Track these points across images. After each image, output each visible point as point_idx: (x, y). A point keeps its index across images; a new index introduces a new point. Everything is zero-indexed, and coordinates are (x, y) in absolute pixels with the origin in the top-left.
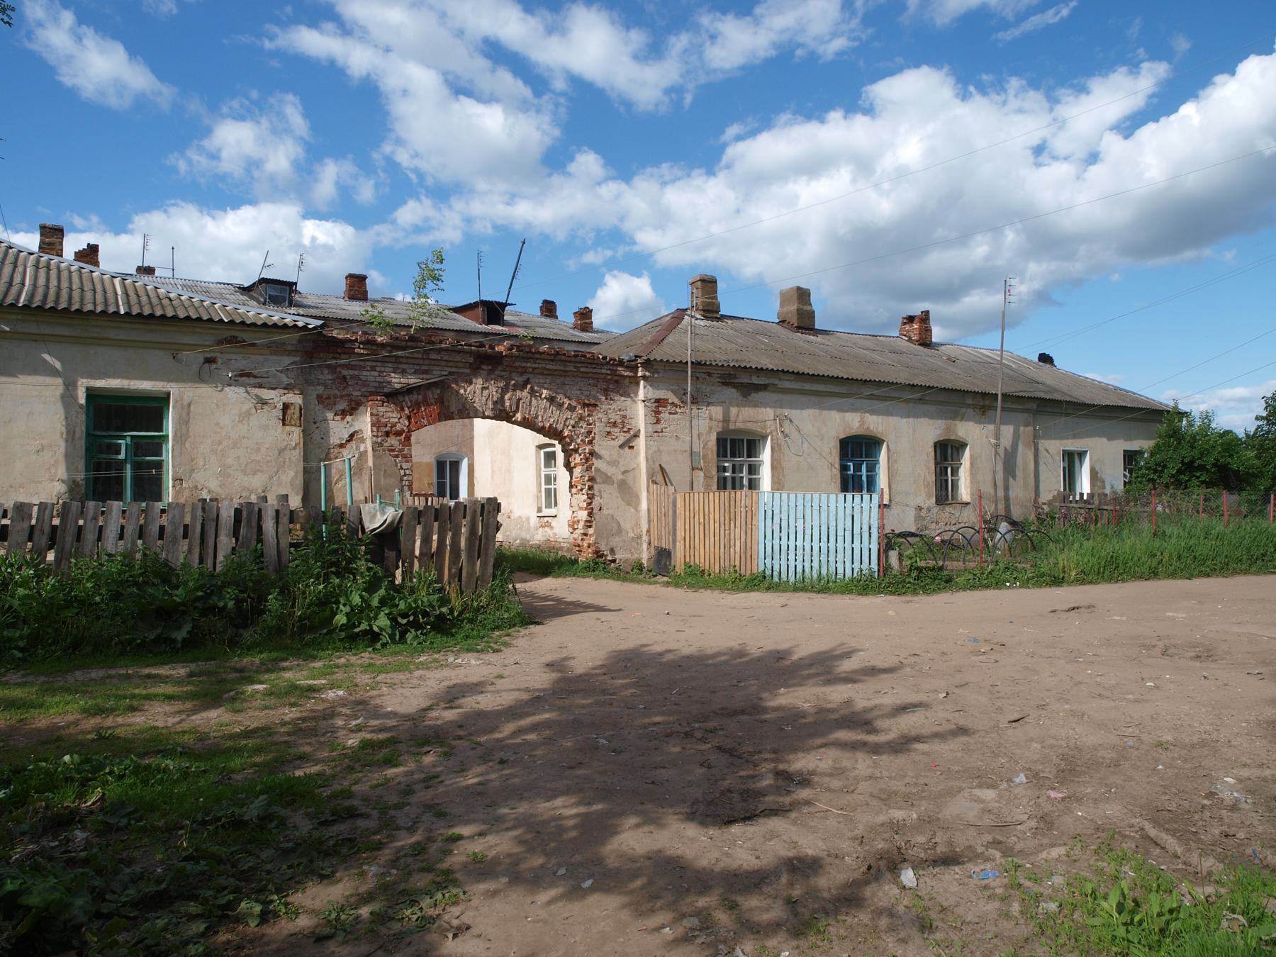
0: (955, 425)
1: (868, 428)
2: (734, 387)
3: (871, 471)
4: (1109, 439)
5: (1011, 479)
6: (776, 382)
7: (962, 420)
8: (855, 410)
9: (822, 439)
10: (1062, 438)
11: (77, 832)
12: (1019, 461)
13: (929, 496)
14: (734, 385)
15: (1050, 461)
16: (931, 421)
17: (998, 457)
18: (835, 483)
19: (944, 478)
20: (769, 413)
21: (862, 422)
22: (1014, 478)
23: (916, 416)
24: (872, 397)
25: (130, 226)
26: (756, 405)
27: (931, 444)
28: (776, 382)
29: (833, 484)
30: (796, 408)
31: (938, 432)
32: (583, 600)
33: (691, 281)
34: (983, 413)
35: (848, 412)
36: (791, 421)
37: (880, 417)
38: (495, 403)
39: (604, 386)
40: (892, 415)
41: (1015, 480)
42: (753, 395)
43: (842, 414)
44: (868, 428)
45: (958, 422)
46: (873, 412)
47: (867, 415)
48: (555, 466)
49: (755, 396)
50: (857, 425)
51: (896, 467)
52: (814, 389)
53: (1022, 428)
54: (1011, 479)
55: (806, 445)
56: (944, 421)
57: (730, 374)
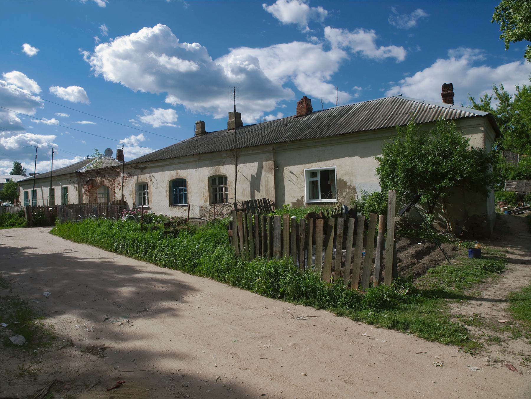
0: (220, 168)
1: (179, 175)
3: (313, 182)
4: (362, 157)
5: (256, 192)
6: (147, 165)
7: (223, 165)
9: (163, 182)
10: (305, 163)
12: (263, 181)
13: (206, 202)
14: (139, 169)
15: (295, 178)
16: (207, 168)
19: (221, 193)
20: (148, 175)
21: (177, 173)
22: (259, 191)
23: (200, 167)
25: (402, 81)
26: (145, 174)
27: (207, 178)
28: (147, 165)
30: (156, 173)
31: (211, 172)
33: (197, 122)
36: (154, 177)
37: (184, 171)
38: (100, 182)
39: (116, 174)
40: (189, 169)
41: (259, 192)
42: (144, 170)
43: (170, 172)
44: (179, 175)
45: (221, 166)
49: (144, 171)
50: (175, 175)
51: (190, 190)
53: (264, 163)
54: (256, 192)
56: (214, 167)
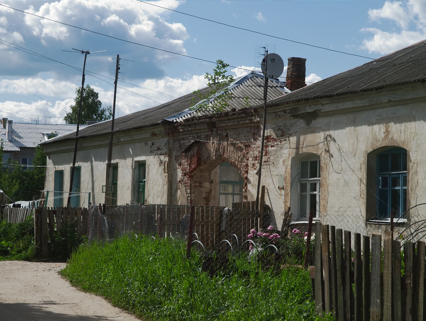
2: (301, 118)
8: (379, 122)
11: (305, 315)
17: (362, 184)
18: (363, 199)
24: (391, 103)
28: (319, 107)
29: (361, 200)
30: (101, 161)
32: (27, 303)
34: (308, 123)
35: (375, 124)
36: (335, 141)
43: (371, 127)
46: (399, 120)
47: (392, 124)
48: (320, 177)
51: (416, 180)
52: (345, 107)
55: (344, 163)
57: (295, 108)
